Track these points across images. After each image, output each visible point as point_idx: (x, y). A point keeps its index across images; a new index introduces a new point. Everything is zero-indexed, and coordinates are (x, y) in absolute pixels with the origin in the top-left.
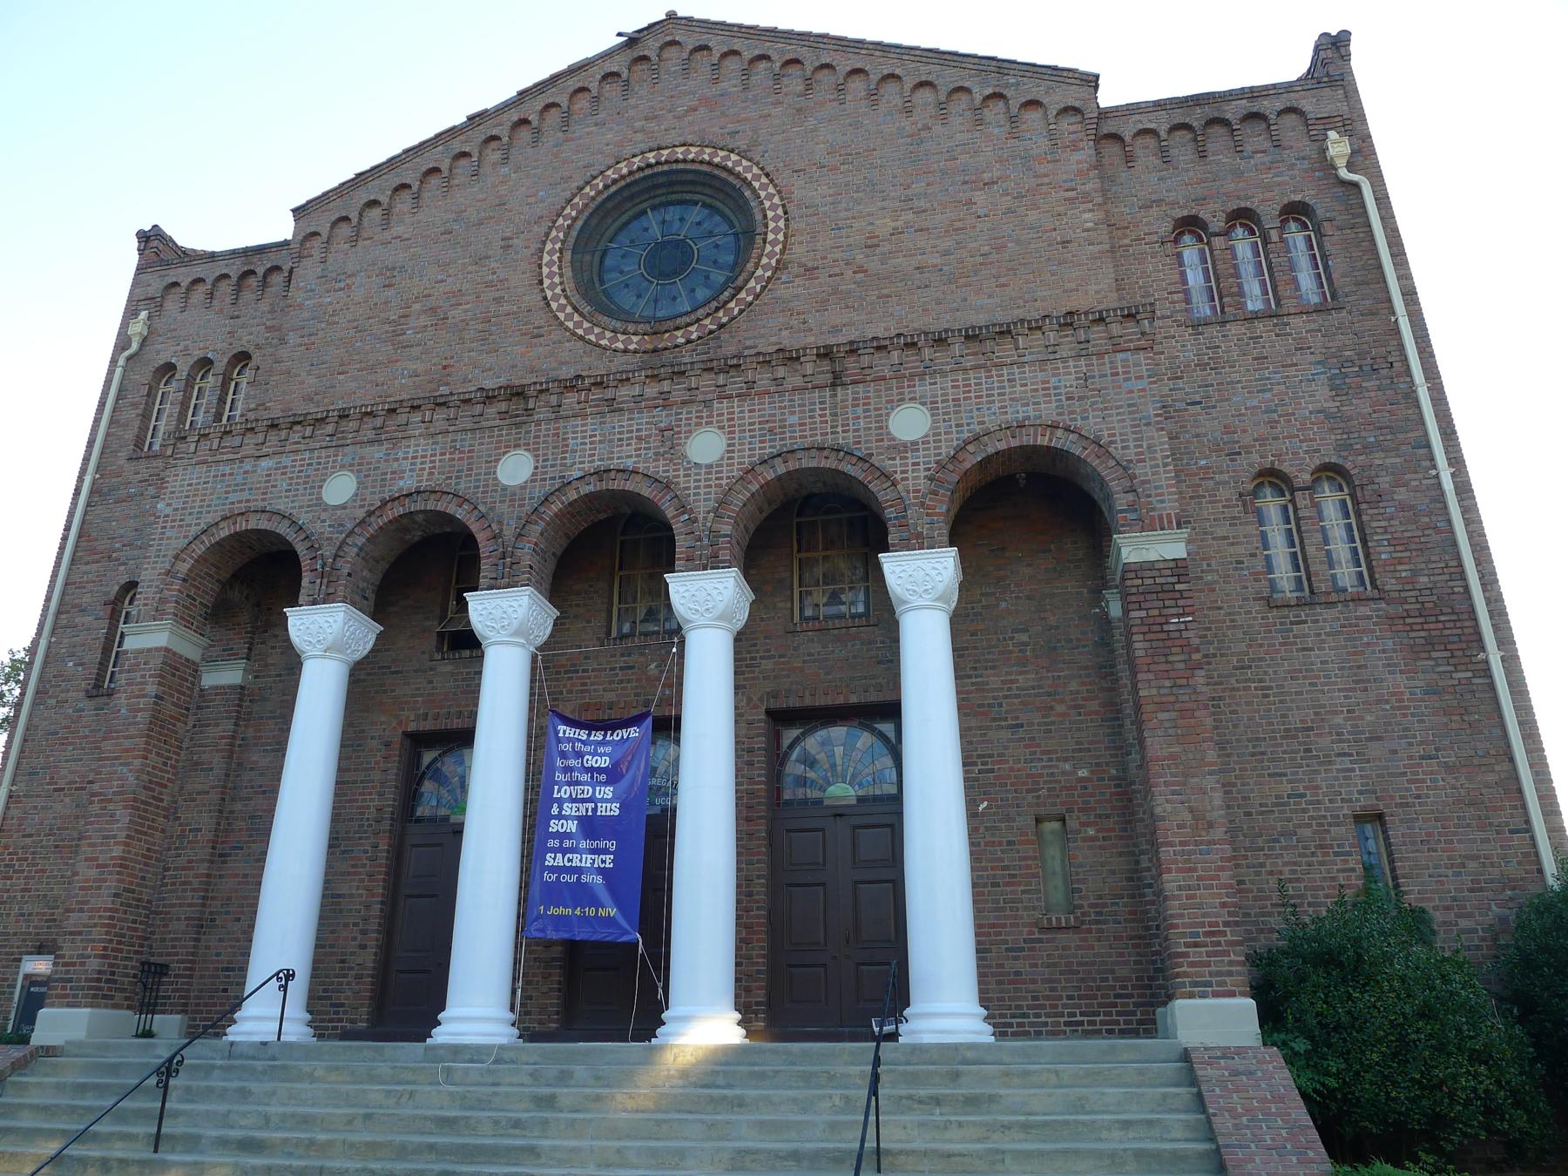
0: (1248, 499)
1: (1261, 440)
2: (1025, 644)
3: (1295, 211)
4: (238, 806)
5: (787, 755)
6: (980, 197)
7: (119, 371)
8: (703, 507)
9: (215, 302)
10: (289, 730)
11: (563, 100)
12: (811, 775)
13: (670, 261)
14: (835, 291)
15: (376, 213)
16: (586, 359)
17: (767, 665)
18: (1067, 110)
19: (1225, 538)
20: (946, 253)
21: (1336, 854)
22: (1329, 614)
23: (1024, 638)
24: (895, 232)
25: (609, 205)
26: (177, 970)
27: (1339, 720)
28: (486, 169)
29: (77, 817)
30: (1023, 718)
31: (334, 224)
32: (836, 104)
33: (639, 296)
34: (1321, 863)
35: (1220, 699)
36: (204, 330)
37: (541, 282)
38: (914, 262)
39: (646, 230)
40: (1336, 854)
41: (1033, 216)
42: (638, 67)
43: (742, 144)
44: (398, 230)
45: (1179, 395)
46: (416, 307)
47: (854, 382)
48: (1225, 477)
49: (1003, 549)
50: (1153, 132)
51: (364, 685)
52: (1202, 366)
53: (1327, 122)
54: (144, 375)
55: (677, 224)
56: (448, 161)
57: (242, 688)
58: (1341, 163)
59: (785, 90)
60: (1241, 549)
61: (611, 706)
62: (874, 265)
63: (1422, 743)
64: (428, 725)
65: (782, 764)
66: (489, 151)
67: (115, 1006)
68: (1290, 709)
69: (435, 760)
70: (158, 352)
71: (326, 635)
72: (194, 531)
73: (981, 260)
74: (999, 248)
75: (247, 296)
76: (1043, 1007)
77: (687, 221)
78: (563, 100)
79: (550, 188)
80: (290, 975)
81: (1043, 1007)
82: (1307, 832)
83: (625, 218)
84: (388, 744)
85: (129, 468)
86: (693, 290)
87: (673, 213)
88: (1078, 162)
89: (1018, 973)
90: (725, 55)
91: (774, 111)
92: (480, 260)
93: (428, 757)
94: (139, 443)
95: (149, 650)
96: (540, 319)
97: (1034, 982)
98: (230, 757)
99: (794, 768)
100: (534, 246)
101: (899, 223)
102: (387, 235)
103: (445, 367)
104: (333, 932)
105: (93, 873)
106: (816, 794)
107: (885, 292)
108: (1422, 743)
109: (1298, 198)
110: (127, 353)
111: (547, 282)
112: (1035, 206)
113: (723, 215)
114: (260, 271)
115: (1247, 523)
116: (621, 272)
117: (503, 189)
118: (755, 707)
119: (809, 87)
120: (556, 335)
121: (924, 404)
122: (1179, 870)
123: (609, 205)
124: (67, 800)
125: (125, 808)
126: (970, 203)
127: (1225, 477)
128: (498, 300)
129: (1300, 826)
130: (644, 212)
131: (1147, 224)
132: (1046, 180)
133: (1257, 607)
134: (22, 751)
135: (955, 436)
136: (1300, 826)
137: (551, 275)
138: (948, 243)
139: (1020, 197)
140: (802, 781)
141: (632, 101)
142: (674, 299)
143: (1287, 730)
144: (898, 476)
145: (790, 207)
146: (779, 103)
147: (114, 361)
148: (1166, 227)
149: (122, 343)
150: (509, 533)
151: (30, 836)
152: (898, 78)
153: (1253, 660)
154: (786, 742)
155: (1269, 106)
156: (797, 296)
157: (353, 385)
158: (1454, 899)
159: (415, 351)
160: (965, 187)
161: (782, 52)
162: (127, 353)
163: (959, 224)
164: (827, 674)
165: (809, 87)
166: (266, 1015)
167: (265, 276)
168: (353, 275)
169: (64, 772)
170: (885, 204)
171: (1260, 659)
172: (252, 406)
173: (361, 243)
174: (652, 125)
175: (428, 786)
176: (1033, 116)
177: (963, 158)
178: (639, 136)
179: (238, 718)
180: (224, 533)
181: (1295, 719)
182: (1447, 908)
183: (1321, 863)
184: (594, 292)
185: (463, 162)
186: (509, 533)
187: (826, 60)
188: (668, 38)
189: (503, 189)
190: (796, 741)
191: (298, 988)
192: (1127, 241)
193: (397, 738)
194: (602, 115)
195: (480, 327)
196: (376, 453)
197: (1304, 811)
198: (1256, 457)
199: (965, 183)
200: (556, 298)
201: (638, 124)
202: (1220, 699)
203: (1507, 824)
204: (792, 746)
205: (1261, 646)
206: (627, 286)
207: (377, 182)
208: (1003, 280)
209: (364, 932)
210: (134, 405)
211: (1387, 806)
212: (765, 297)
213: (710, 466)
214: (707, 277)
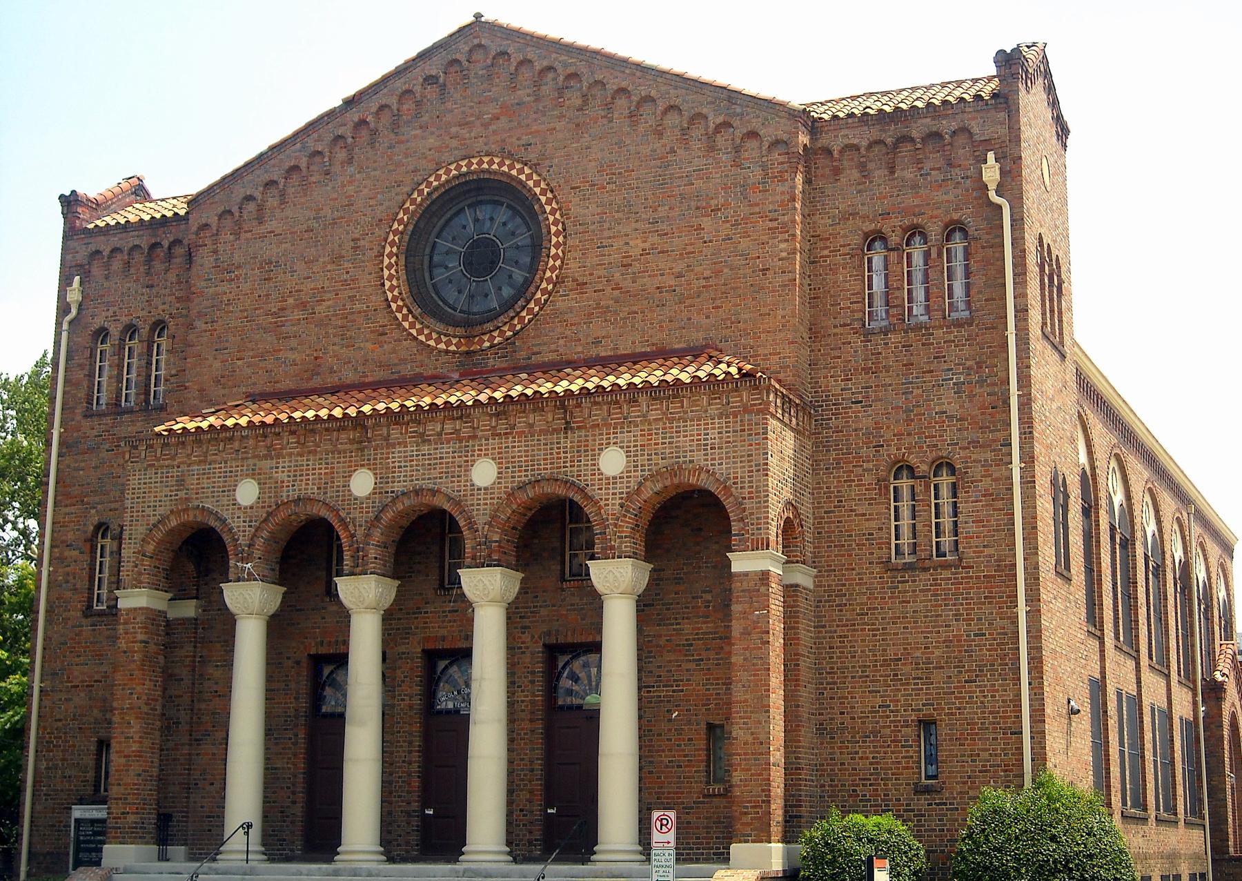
0: (882, 484)
1: (899, 435)
2: (709, 602)
3: (954, 228)
4: (203, 706)
5: (560, 674)
6: (706, 223)
7: (64, 335)
8: (481, 520)
9: (132, 270)
10: (233, 651)
11: (393, 102)
12: (575, 688)
13: (483, 258)
14: (598, 306)
15: (251, 207)
16: (419, 358)
17: (544, 612)
18: (777, 143)
19: (864, 515)
20: (680, 276)
21: (903, 746)
22: (923, 576)
23: (708, 597)
24: (644, 252)
25: (434, 208)
26: (183, 818)
27: (918, 654)
28: (337, 168)
29: (91, 707)
30: (704, 655)
31: (220, 216)
32: (605, 121)
33: (460, 292)
34: (893, 752)
35: (845, 636)
36: (131, 300)
37: (383, 285)
38: (657, 282)
39: (464, 227)
40: (903, 746)
41: (744, 244)
42: (452, 69)
43: (532, 156)
44: (272, 225)
45: (847, 394)
46: (291, 301)
47: (579, 428)
48: (870, 465)
49: (700, 529)
50: (856, 148)
51: (277, 628)
52: (866, 370)
53: (987, 144)
54: (84, 339)
55: (488, 224)
56: (305, 159)
57: (196, 620)
58: (992, 187)
59: (567, 102)
60: (873, 524)
61: (444, 638)
62: (627, 284)
63: (967, 671)
64: (323, 650)
65: (558, 679)
66: (337, 149)
67: (147, 843)
68: (888, 645)
69: (332, 672)
70: (93, 317)
71: (250, 601)
72: (153, 520)
73: (703, 283)
74: (718, 273)
75: (158, 266)
76: (702, 843)
77: (495, 221)
78: (393, 102)
79: (383, 196)
80: (250, 826)
81: (702, 843)
82: (888, 731)
83: (448, 215)
84: (298, 663)
85: (86, 424)
86: (500, 289)
87: (483, 213)
88: (782, 193)
89: (689, 823)
90: (521, 63)
91: (559, 126)
92: (337, 259)
93: (326, 671)
94: (89, 409)
95: (135, 609)
96: (382, 319)
97: (698, 828)
98: (194, 670)
99: (565, 683)
100: (376, 249)
101: (647, 245)
102: (262, 229)
103: (316, 358)
104: (274, 792)
105: (123, 760)
106: (579, 701)
107: (635, 308)
108: (967, 671)
109: (956, 216)
110: (68, 318)
111: (387, 284)
112: (746, 235)
113: (523, 218)
114: (166, 244)
115: (879, 503)
116: (446, 267)
117: (350, 189)
118: (536, 642)
119: (585, 102)
120: (396, 334)
121: (622, 447)
122: (743, 770)
123: (434, 208)
124: (82, 695)
125: (137, 718)
126: (700, 228)
127: (870, 465)
128: (352, 298)
129: (884, 727)
130: (462, 210)
131: (845, 236)
132: (757, 209)
133: (877, 569)
134: (44, 657)
135: (639, 473)
136: (884, 727)
137: (390, 278)
138: (680, 267)
139: (737, 224)
140: (570, 692)
141: (449, 105)
142: (486, 296)
143: (885, 660)
144: (602, 503)
145: (569, 223)
146: (562, 116)
147: (59, 324)
148: (856, 240)
149: (63, 308)
150: (360, 532)
151: (60, 720)
152: (654, 100)
153: (869, 609)
154: (561, 665)
155: (947, 126)
156: (571, 308)
157: (249, 371)
158: (969, 777)
159: (293, 343)
160: (698, 213)
161: (565, 65)
162: (68, 318)
163: (690, 249)
164: (583, 619)
165: (585, 102)
166: (236, 843)
167: (169, 248)
168: (239, 267)
169: (76, 673)
170: (638, 225)
171: (875, 608)
172: (173, 372)
173: (243, 236)
174: (464, 132)
175: (328, 691)
176: (752, 144)
177: (699, 184)
178: (454, 143)
179: (196, 642)
180: (174, 523)
181: (891, 652)
182: (965, 783)
183: (893, 752)
184: (426, 300)
185: (317, 159)
186: (360, 532)
187: (599, 77)
188: (476, 41)
189: (350, 189)
190: (567, 664)
191: (255, 833)
192: (826, 252)
193: (305, 661)
194: (426, 118)
195: (340, 323)
196: (267, 464)
197: (888, 717)
198: (893, 450)
199: (698, 208)
200: (395, 299)
201: (454, 130)
202: (845, 636)
203: (1010, 728)
204: (564, 668)
205: (876, 598)
206: (450, 282)
207: (250, 177)
208: (718, 303)
209: (294, 793)
210: (81, 366)
211: (939, 715)
212: (548, 309)
213: (486, 489)
214: (510, 277)
